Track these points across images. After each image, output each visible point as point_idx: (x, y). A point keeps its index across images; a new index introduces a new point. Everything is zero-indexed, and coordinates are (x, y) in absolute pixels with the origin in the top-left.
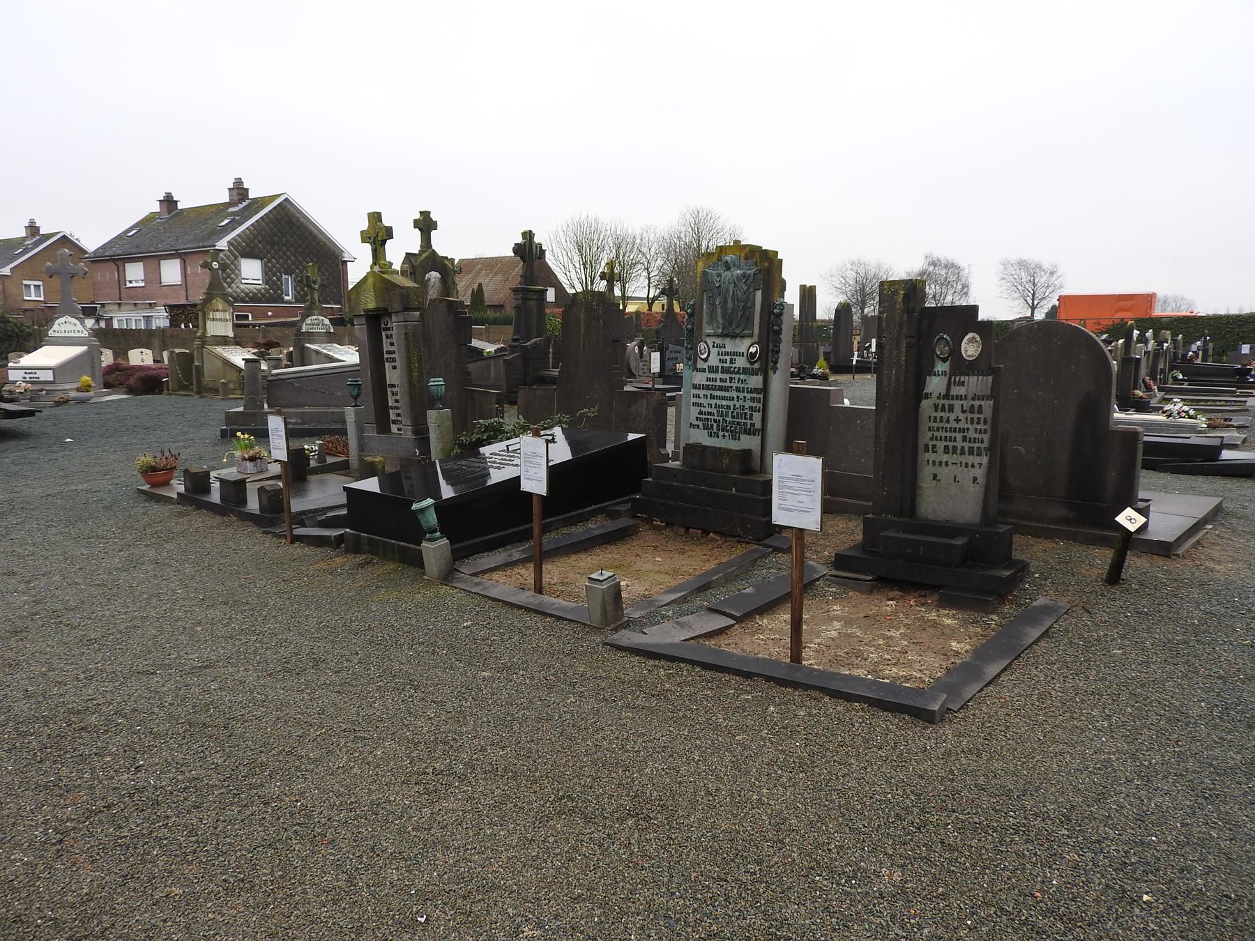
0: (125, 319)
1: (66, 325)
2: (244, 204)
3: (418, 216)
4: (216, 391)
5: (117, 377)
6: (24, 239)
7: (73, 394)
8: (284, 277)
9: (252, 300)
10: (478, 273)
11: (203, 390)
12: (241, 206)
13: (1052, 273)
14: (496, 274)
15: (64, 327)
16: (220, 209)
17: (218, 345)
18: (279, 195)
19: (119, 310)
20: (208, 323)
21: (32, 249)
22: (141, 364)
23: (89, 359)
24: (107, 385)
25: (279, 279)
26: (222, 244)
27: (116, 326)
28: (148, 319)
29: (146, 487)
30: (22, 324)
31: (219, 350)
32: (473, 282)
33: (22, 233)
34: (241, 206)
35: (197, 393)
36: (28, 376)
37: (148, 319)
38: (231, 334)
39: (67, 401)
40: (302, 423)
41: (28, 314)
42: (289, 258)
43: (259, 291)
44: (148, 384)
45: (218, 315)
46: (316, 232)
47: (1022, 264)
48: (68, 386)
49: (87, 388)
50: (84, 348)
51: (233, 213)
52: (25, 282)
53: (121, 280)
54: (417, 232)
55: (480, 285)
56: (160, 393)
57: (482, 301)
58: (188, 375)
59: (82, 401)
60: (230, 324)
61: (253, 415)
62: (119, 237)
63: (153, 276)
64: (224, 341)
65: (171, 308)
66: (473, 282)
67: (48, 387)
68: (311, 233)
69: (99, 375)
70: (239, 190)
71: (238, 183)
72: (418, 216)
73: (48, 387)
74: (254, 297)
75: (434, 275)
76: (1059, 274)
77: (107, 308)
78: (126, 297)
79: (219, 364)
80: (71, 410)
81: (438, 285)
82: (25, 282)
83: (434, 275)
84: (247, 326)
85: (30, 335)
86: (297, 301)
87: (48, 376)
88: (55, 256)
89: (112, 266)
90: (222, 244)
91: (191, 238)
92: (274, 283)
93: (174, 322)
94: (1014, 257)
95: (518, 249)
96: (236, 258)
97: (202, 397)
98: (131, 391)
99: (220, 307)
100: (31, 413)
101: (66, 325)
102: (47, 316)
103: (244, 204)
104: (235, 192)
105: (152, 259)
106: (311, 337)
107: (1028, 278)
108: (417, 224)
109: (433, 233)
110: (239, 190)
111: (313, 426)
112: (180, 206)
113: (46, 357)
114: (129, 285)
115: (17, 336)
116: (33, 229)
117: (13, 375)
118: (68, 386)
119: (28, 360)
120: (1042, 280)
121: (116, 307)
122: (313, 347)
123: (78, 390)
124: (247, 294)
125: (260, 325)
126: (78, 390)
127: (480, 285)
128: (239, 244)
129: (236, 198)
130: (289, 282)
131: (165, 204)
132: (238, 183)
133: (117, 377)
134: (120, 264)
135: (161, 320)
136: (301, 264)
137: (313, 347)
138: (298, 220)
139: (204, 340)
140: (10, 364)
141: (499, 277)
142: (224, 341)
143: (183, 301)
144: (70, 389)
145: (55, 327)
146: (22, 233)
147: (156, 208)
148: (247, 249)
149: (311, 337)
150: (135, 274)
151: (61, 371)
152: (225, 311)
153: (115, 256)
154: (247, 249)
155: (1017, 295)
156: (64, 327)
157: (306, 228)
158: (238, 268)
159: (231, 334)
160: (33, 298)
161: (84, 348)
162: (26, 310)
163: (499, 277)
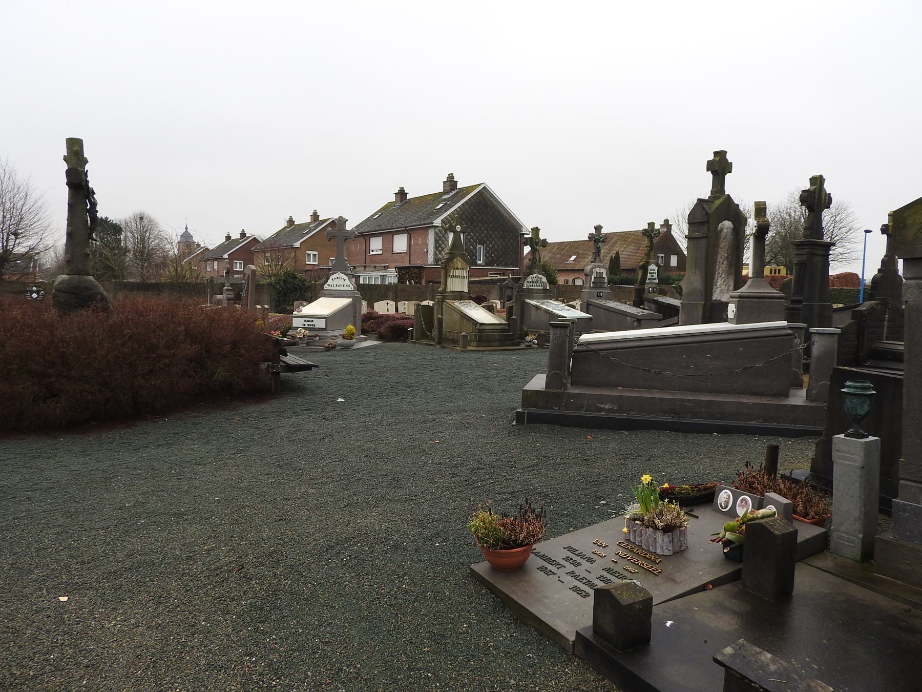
0: (371, 277)
1: (339, 281)
3: (711, 157)
4: (455, 342)
5: (372, 325)
7: (340, 341)
10: (614, 244)
11: (443, 341)
14: (629, 244)
16: (436, 197)
17: (455, 299)
19: (365, 271)
20: (449, 279)
22: (386, 313)
23: (353, 308)
24: (364, 332)
25: (475, 248)
26: (438, 222)
27: (362, 282)
28: (383, 277)
29: (482, 568)
30: (305, 280)
31: (457, 304)
32: (610, 251)
35: (439, 343)
36: (307, 323)
37: (383, 277)
38: (466, 290)
39: (334, 347)
40: (620, 410)
44: (394, 331)
45: (458, 273)
46: (503, 212)
48: (336, 333)
49: (350, 336)
50: (349, 300)
51: (445, 199)
53: (367, 249)
54: (709, 175)
55: (617, 253)
56: (405, 341)
58: (430, 326)
59: (346, 348)
60: (466, 281)
61: (558, 396)
62: (368, 220)
63: (388, 246)
64: (460, 296)
65: (400, 269)
66: (610, 251)
67: (321, 334)
68: (500, 212)
69: (359, 321)
70: (451, 182)
72: (711, 157)
73: (321, 334)
75: (727, 224)
77: (357, 269)
78: (370, 262)
79: (457, 317)
80: (339, 357)
81: (730, 236)
83: (727, 224)
85: (309, 287)
86: (486, 265)
87: (321, 324)
88: (331, 234)
89: (362, 240)
90: (438, 222)
91: (416, 218)
92: (471, 251)
93: (401, 279)
95: (591, 237)
97: (443, 347)
98: (381, 337)
99: (460, 266)
100: (307, 368)
101: (339, 281)
102: (325, 274)
104: (448, 184)
105: (388, 235)
106: (530, 293)
108: (711, 166)
109: (728, 177)
110: (451, 182)
111: (633, 415)
112: (409, 197)
113: (322, 307)
114: (372, 253)
115: (301, 289)
116: (315, 216)
117: (297, 322)
118: (336, 333)
119: (309, 309)
121: (362, 269)
122: (533, 302)
123: (344, 337)
126: (344, 337)
127: (617, 253)
129: (448, 188)
130: (481, 249)
133: (372, 325)
134: (367, 238)
135: (392, 277)
136: (491, 236)
137: (533, 302)
138: (491, 202)
139: (446, 295)
140: (295, 313)
141: (631, 247)
142: (460, 296)
143: (407, 265)
144: (336, 335)
145: (330, 282)
147: (393, 199)
149: (530, 293)
150: (376, 245)
151: (332, 319)
152: (463, 269)
153: (365, 233)
157: (497, 209)
159: (466, 290)
160: (311, 263)
161: (349, 300)
163: (631, 247)
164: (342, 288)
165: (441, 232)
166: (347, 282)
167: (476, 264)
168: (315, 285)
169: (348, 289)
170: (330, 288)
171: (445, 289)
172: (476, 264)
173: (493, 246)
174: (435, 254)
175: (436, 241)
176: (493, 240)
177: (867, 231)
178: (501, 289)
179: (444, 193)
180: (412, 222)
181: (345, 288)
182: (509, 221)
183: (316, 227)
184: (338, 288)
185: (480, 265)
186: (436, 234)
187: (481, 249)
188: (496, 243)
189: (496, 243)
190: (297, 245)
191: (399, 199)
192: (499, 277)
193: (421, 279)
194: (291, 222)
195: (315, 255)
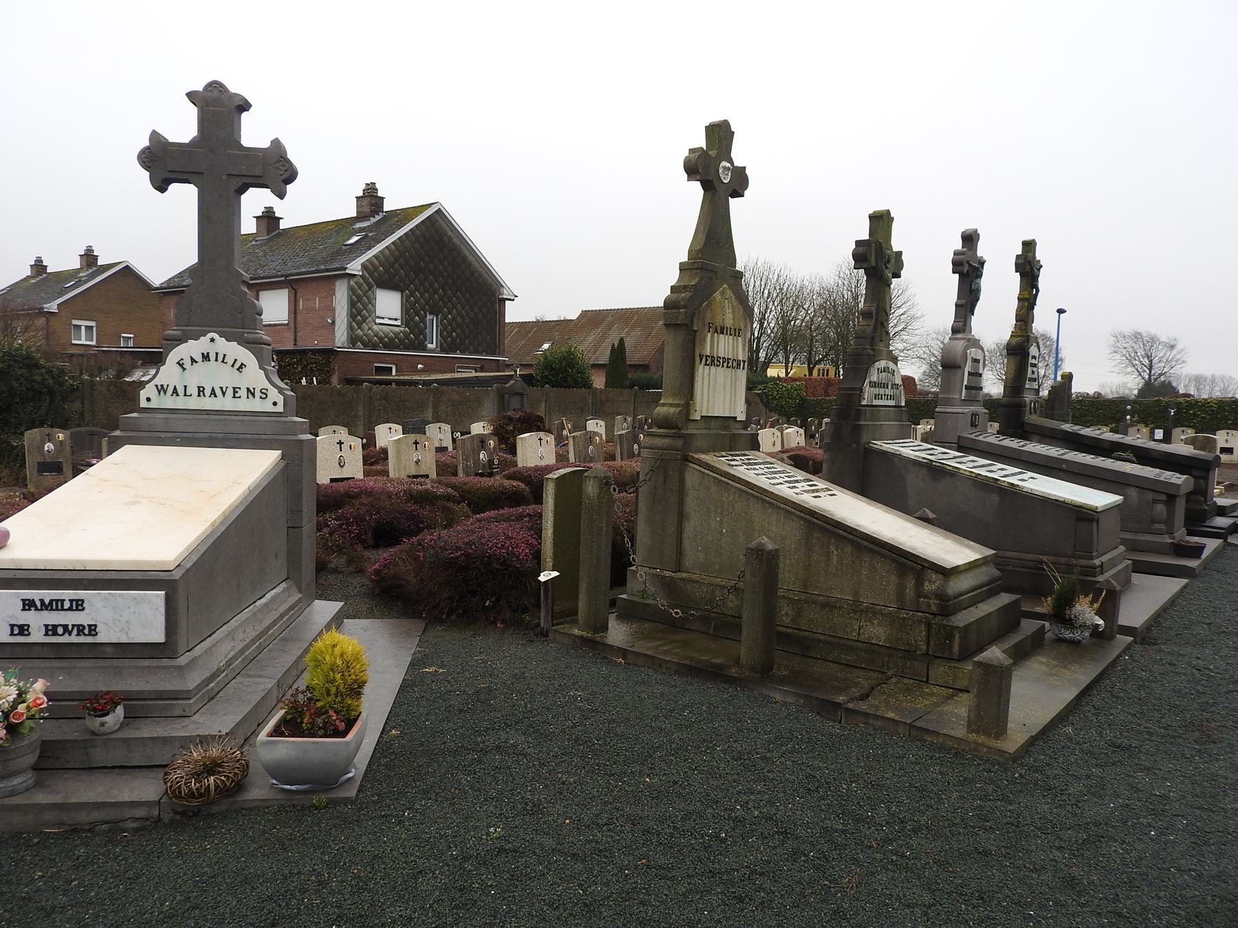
2: (377, 218)
6: (77, 271)
8: (429, 317)
9: (386, 347)
10: (609, 327)
12: (373, 220)
13: (1172, 347)
14: (633, 327)
15: (198, 376)
16: (343, 226)
18: (430, 205)
20: (702, 371)
21: (86, 282)
25: (423, 320)
26: (355, 267)
33: (76, 264)
34: (373, 220)
36: (37, 621)
41: (75, 360)
42: (436, 292)
43: (396, 335)
46: (471, 258)
47: (1137, 336)
51: (361, 230)
52: (75, 322)
55: (622, 340)
57: (623, 358)
68: (465, 258)
70: (370, 199)
71: (371, 190)
74: (390, 343)
76: (1179, 347)
82: (75, 322)
84: (388, 383)
85: (73, 390)
86: (442, 351)
87: (141, 619)
90: (355, 267)
92: (417, 325)
94: (1128, 329)
96: (370, 287)
103: (377, 218)
104: (366, 201)
107: (1141, 349)
110: (370, 199)
115: (51, 393)
116: (89, 258)
120: (1158, 354)
124: (381, 339)
125: (430, 382)
127: (622, 340)
128: (376, 269)
129: (367, 210)
130: (433, 324)
131: (264, 223)
132: (371, 190)
138: (450, 239)
143: (290, 347)
145: (168, 373)
146: (76, 264)
148: (384, 275)
154: (384, 275)
155: (1130, 369)
156: (198, 376)
157: (459, 252)
158: (372, 301)
160: (83, 342)
162: (72, 355)
163: (637, 332)
164: (227, 403)
165: (360, 287)
166: (254, 375)
167: (425, 349)
168: (92, 383)
169: (256, 405)
170: (168, 402)
171: (687, 407)
172: (425, 349)
173: (454, 319)
174: (350, 328)
175: (352, 304)
176: (454, 307)
177: (1061, 311)
178: (502, 397)
179: (361, 217)
180: (299, 265)
181: (244, 404)
182: (481, 276)
183: (92, 276)
184: (208, 403)
185: (432, 351)
186: (351, 289)
187: (433, 324)
188: (459, 314)
189: (459, 314)
190: (53, 307)
191: (264, 230)
192: (474, 374)
193: (329, 373)
194: (39, 267)
195: (89, 328)
